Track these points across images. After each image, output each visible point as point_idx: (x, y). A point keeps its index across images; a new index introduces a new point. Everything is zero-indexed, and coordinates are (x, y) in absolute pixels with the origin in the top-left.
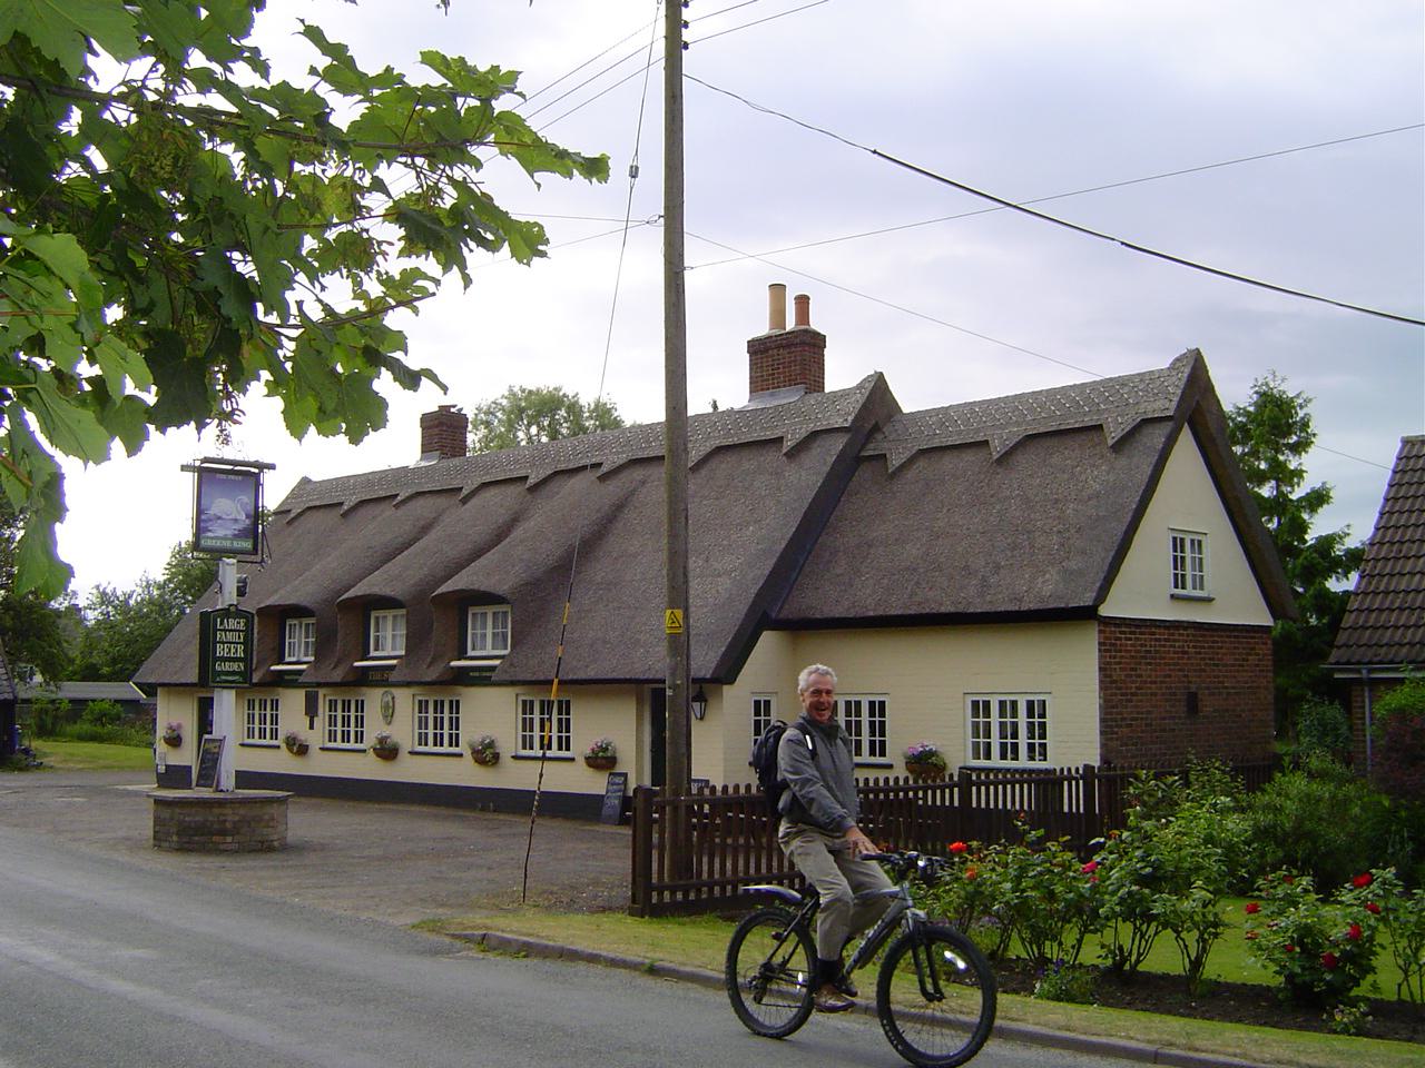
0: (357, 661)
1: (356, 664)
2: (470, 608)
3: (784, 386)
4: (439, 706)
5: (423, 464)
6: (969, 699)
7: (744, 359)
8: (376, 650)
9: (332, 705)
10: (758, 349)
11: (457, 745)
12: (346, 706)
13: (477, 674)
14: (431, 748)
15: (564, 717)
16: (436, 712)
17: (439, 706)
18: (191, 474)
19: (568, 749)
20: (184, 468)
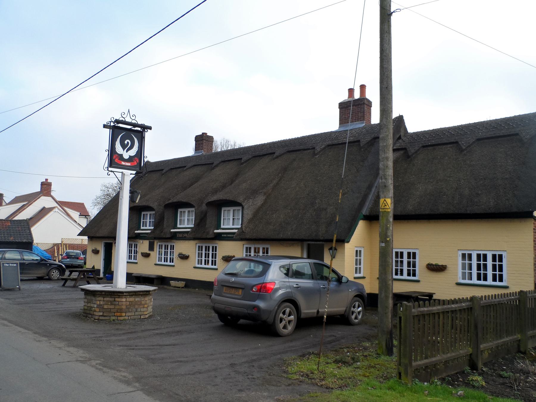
0: (172, 229)
1: (172, 230)
2: (179, 209)
3: (355, 121)
4: (207, 249)
5: (342, 129)
6: (460, 253)
7: (337, 111)
8: (180, 224)
9: (160, 247)
10: (343, 106)
11: (136, 260)
12: (166, 247)
13: (225, 235)
14: (163, 263)
15: (200, 252)
16: (206, 251)
17: (207, 249)
18: (109, 129)
19: (215, 265)
20: (105, 126)
